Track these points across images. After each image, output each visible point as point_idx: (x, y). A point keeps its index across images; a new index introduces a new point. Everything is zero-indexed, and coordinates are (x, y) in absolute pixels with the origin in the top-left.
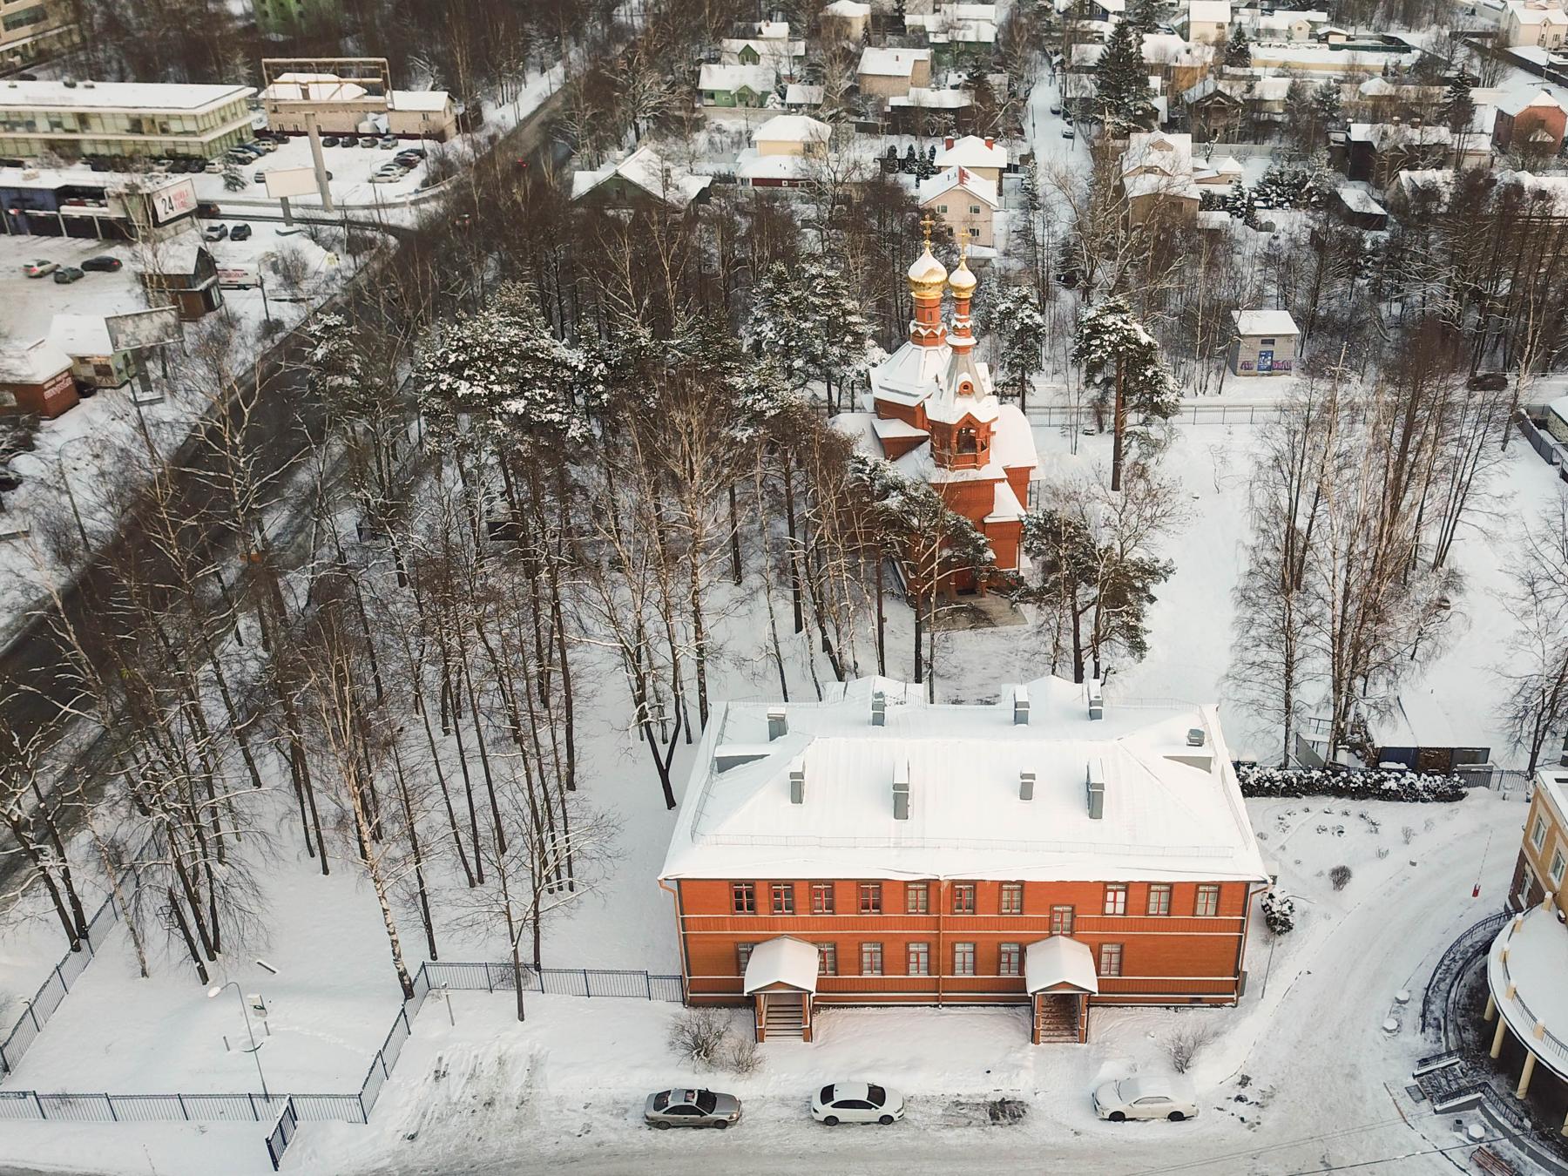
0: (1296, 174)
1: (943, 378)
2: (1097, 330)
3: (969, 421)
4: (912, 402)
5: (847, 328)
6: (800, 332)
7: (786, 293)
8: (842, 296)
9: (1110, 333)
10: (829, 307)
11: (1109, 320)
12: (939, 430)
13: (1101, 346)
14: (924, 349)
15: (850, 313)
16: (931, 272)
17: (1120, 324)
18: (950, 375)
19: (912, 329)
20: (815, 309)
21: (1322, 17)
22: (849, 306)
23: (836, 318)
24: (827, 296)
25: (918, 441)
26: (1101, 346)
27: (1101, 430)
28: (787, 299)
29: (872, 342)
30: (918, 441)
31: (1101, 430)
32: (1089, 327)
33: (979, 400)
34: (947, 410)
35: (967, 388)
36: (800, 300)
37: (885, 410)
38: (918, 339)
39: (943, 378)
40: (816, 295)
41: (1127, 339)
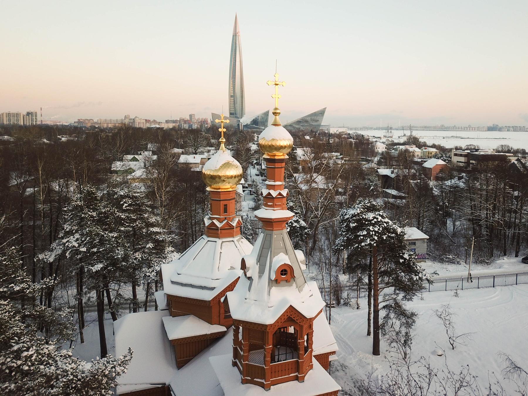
0: (366, 184)
1: (251, 262)
2: (362, 224)
3: (292, 315)
4: (208, 296)
5: (150, 236)
6: (102, 242)
7: (94, 210)
8: (146, 211)
9: (373, 225)
10: (135, 221)
11: (370, 216)
12: (253, 335)
13: (368, 235)
14: (219, 241)
15: (153, 225)
16: (227, 165)
17: (380, 218)
18: (261, 259)
19: (207, 222)
20: (119, 222)
21: (339, 154)
22: (153, 220)
23: (141, 228)
24: (133, 212)
25: (216, 338)
26: (368, 235)
27: (338, 303)
28: (94, 214)
29: (171, 249)
30: (216, 338)
31: (338, 303)
32: (356, 221)
33: (300, 288)
34: (260, 306)
35: (286, 274)
36: (106, 215)
37: (179, 306)
38: (213, 232)
39: (251, 262)
40: (124, 211)
41: (387, 230)
